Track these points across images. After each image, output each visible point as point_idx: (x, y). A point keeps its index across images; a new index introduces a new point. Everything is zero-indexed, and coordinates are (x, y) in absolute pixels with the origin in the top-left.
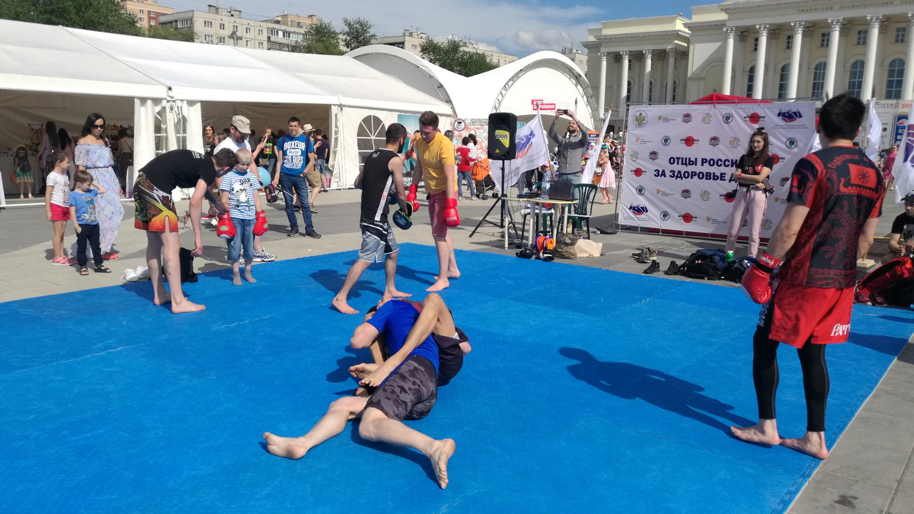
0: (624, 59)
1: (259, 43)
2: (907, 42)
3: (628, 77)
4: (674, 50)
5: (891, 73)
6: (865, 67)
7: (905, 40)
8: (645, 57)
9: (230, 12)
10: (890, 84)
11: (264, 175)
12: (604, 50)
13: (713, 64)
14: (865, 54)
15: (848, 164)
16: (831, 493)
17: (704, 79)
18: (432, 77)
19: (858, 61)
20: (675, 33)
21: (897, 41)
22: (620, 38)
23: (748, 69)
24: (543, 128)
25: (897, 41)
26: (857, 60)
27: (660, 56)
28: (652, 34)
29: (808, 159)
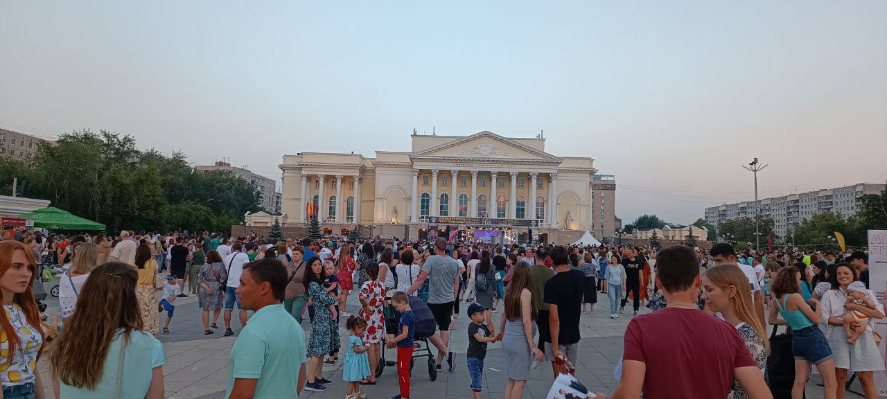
1: (309, 178)
9: (411, 166)
23: (439, 196)
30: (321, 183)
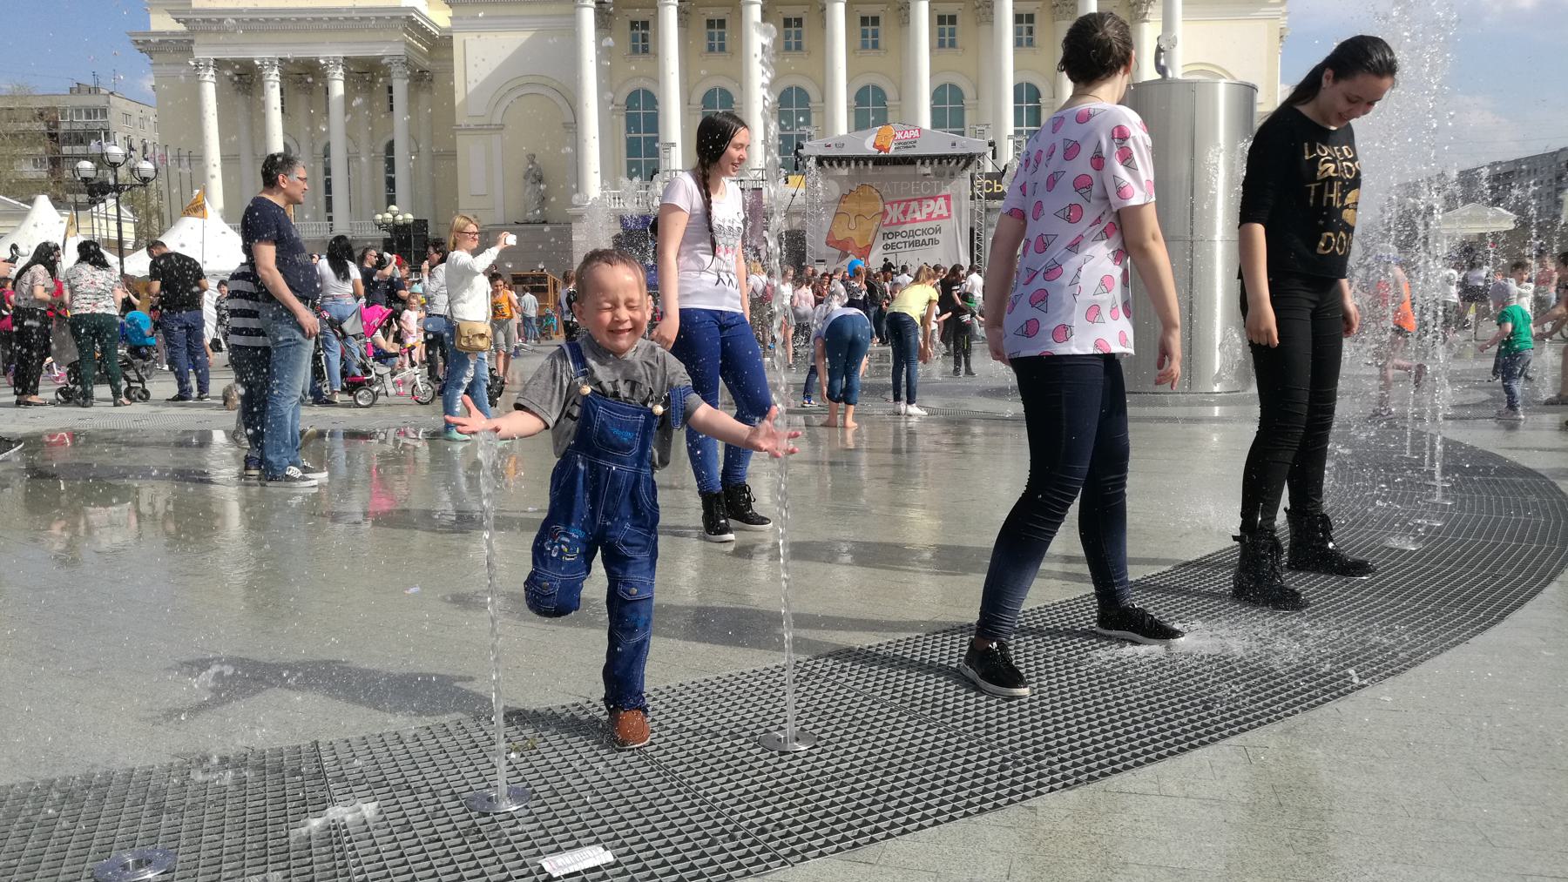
0: (265, 78)
2: (656, 55)
3: (285, 133)
4: (405, 60)
5: (632, 122)
6: (660, 126)
7: (651, 49)
8: (261, 77)
10: (633, 147)
11: (485, 587)
12: (204, 52)
13: (529, 90)
14: (657, 77)
15: (349, 263)
16: (112, 524)
17: (501, 127)
18: (347, 135)
19: (790, 89)
20: (403, 15)
21: (711, 49)
22: (251, 20)
24: (920, 331)
25: (711, 49)
26: (635, 88)
27: (365, 74)
28: (325, 16)
29: (1122, 363)
30: (400, 87)
